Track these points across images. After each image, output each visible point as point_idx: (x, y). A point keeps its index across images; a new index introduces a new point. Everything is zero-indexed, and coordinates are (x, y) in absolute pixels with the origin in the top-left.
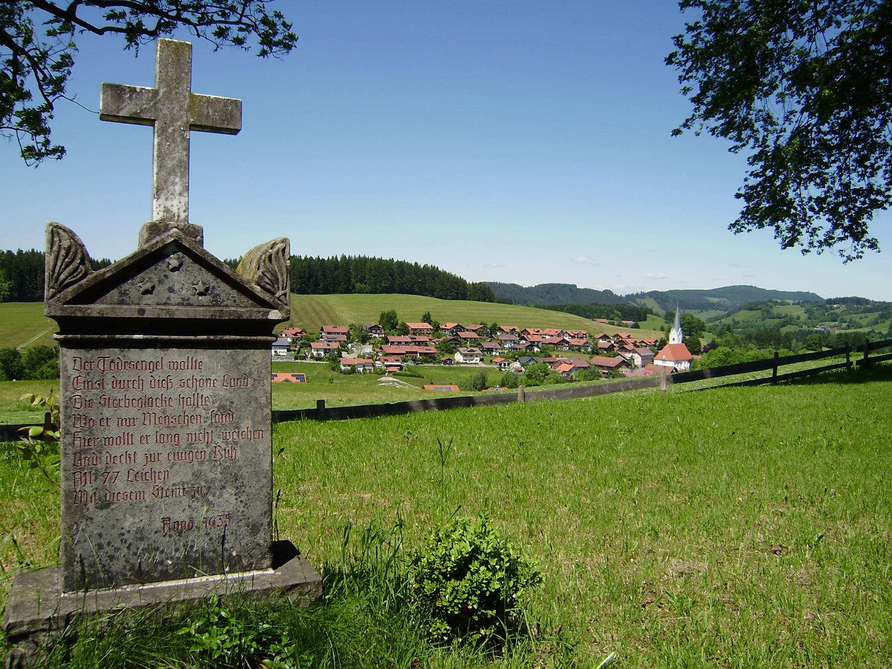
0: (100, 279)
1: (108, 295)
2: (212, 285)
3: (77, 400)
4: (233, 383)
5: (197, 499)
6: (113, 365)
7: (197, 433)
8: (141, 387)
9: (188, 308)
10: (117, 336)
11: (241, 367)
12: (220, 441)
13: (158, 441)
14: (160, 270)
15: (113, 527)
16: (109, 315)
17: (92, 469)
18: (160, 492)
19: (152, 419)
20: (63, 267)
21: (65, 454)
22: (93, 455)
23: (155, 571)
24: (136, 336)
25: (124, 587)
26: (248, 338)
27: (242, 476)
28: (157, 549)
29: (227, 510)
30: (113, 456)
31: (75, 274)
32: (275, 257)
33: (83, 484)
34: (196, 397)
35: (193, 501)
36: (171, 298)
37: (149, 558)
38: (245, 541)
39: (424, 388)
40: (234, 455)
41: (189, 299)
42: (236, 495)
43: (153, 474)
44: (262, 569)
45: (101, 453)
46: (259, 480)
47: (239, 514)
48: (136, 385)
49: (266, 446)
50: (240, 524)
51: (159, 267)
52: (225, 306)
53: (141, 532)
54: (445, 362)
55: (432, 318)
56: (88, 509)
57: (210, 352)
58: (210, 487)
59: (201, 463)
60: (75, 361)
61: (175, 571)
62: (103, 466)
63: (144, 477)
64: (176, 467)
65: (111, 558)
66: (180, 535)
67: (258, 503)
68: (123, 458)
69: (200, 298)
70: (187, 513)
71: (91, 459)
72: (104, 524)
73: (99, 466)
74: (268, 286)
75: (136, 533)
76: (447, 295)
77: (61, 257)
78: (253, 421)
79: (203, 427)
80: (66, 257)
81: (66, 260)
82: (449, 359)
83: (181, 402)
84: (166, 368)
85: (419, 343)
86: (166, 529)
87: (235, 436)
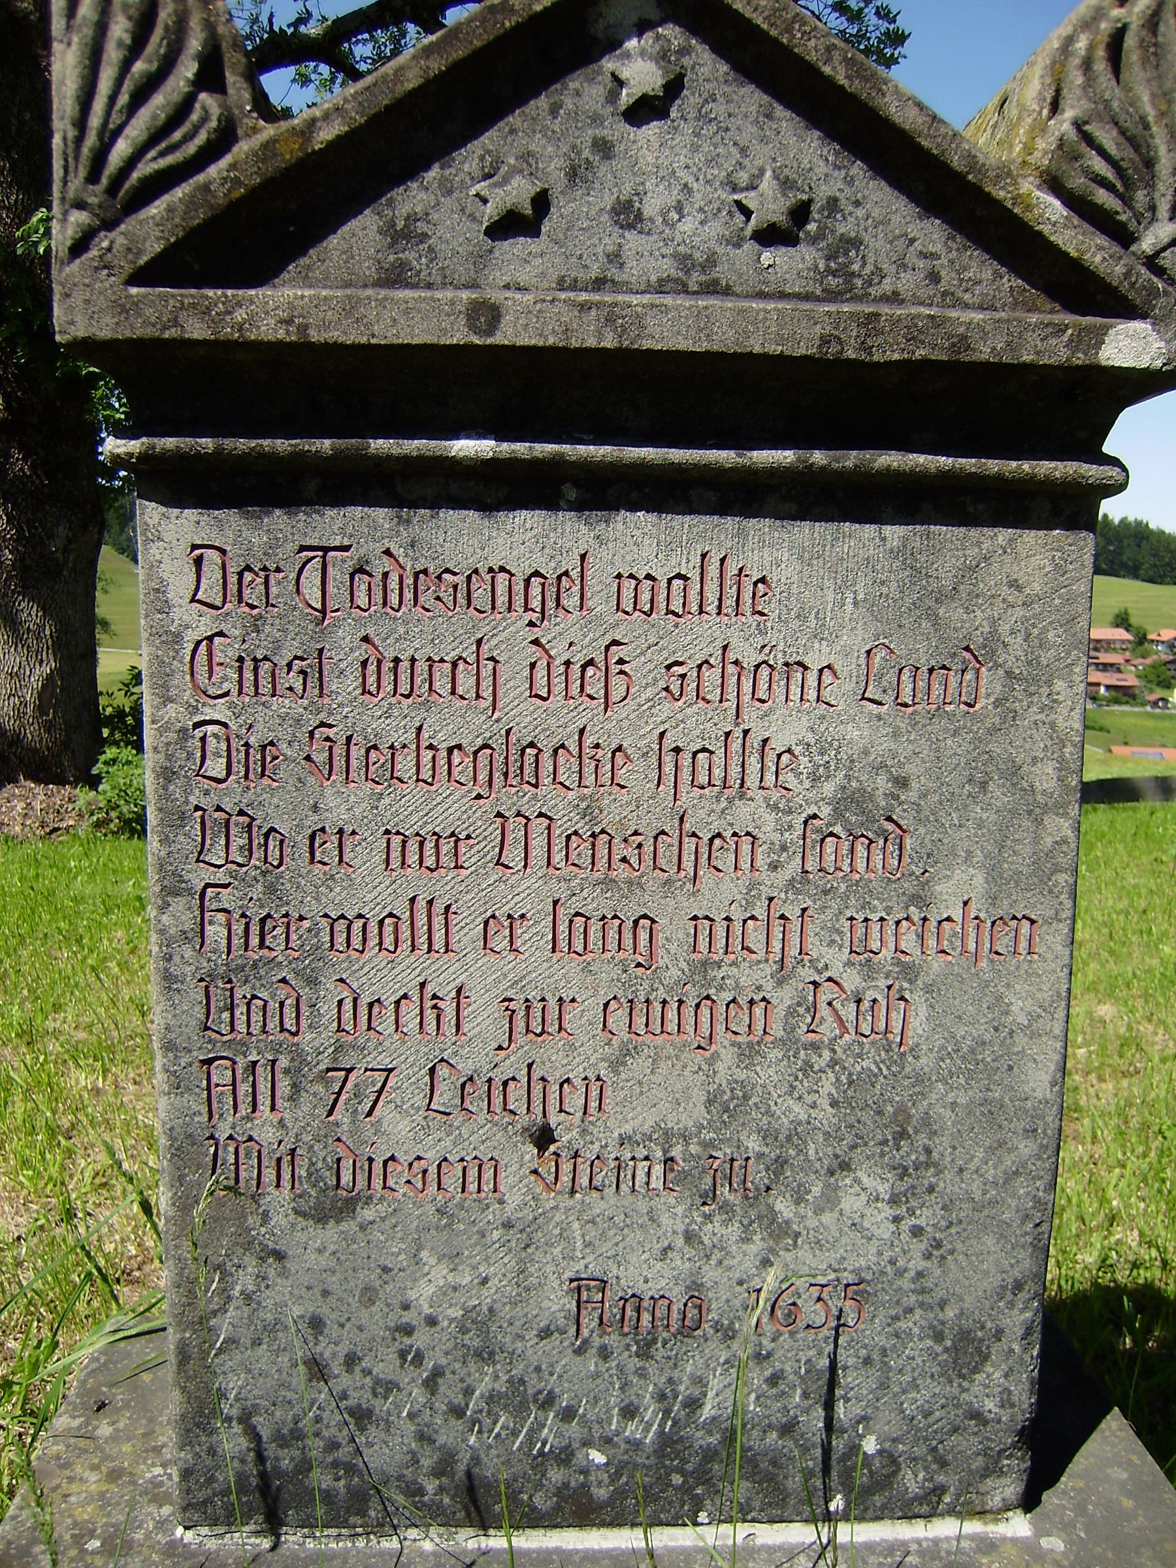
0: (289, 153)
1: (333, 241)
2: (823, 192)
3: (212, 743)
4: (907, 689)
5: (726, 1208)
6: (362, 581)
7: (737, 915)
8: (487, 693)
9: (713, 301)
10: (379, 445)
11: (952, 613)
12: (836, 959)
13: (563, 944)
14: (575, 115)
15: (369, 1295)
16: (335, 335)
17: (277, 1049)
18: (566, 1167)
19: (538, 843)
20: (123, 99)
21: (168, 979)
22: (283, 990)
23: (539, 1486)
24: (465, 447)
25: (413, 1533)
26: (993, 466)
27: (926, 1121)
28: (549, 1401)
29: (852, 1263)
30: (365, 1000)
31: (177, 135)
32: (1142, 44)
33: (244, 1109)
34: (735, 746)
35: (708, 1217)
36: (628, 253)
37: (515, 1433)
38: (922, 1397)
39: (1110, 751)
40: (896, 1027)
41: (711, 261)
42: (894, 1201)
43: (537, 1088)
44: (981, 1513)
45: (313, 982)
46: (1001, 1144)
47: (905, 1283)
48: (466, 683)
49: (1045, 995)
50: (902, 1325)
51: (569, 103)
52: (885, 299)
53: (483, 1327)
54: (1155, 704)
55: (1134, 621)
56: (265, 1216)
57: (806, 532)
58: (781, 1163)
59: (749, 1054)
60: (198, 562)
61: (620, 1494)
62: (327, 1036)
63: (497, 1100)
64: (638, 1066)
65: (362, 1416)
66: (645, 1351)
67: (990, 1241)
68: (410, 1012)
69: (767, 257)
70: (680, 1263)
71: (273, 1006)
72: (333, 1281)
73: (306, 1038)
74: (1102, 197)
75: (463, 1330)
76: (1165, 576)
77: (113, 55)
78: (993, 873)
79: (766, 891)
80: (135, 49)
81: (139, 67)
82: (1162, 699)
83: (669, 768)
84: (601, 604)
85: (1106, 667)
86: (589, 1322)
87: (909, 941)
